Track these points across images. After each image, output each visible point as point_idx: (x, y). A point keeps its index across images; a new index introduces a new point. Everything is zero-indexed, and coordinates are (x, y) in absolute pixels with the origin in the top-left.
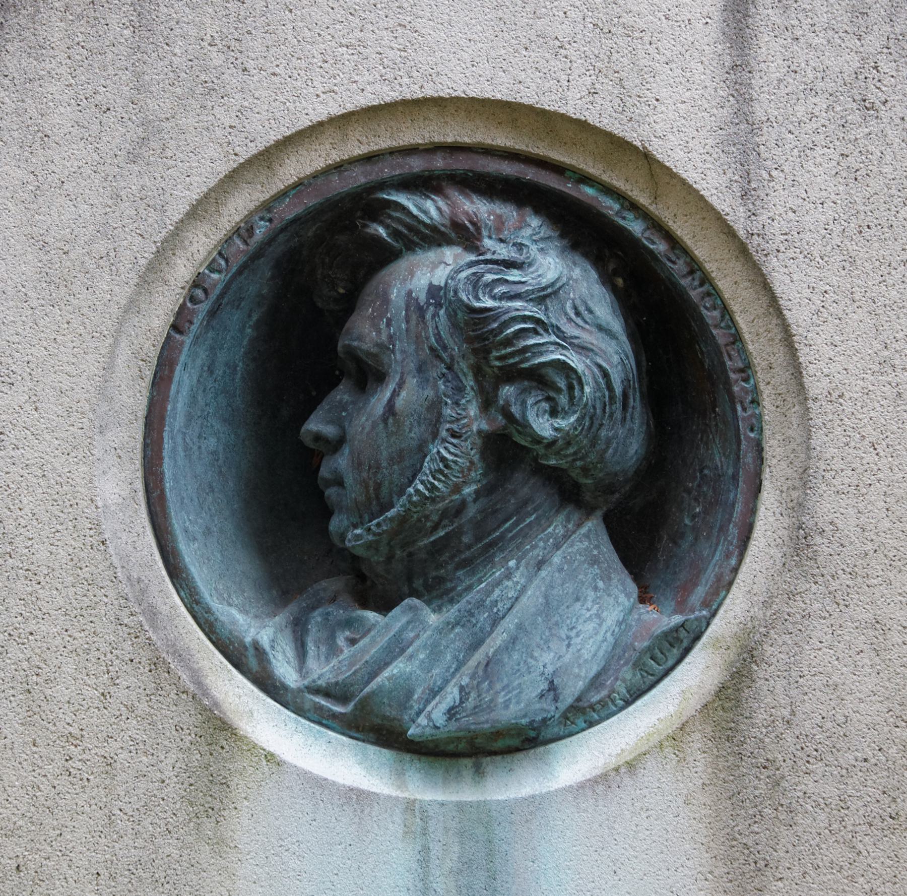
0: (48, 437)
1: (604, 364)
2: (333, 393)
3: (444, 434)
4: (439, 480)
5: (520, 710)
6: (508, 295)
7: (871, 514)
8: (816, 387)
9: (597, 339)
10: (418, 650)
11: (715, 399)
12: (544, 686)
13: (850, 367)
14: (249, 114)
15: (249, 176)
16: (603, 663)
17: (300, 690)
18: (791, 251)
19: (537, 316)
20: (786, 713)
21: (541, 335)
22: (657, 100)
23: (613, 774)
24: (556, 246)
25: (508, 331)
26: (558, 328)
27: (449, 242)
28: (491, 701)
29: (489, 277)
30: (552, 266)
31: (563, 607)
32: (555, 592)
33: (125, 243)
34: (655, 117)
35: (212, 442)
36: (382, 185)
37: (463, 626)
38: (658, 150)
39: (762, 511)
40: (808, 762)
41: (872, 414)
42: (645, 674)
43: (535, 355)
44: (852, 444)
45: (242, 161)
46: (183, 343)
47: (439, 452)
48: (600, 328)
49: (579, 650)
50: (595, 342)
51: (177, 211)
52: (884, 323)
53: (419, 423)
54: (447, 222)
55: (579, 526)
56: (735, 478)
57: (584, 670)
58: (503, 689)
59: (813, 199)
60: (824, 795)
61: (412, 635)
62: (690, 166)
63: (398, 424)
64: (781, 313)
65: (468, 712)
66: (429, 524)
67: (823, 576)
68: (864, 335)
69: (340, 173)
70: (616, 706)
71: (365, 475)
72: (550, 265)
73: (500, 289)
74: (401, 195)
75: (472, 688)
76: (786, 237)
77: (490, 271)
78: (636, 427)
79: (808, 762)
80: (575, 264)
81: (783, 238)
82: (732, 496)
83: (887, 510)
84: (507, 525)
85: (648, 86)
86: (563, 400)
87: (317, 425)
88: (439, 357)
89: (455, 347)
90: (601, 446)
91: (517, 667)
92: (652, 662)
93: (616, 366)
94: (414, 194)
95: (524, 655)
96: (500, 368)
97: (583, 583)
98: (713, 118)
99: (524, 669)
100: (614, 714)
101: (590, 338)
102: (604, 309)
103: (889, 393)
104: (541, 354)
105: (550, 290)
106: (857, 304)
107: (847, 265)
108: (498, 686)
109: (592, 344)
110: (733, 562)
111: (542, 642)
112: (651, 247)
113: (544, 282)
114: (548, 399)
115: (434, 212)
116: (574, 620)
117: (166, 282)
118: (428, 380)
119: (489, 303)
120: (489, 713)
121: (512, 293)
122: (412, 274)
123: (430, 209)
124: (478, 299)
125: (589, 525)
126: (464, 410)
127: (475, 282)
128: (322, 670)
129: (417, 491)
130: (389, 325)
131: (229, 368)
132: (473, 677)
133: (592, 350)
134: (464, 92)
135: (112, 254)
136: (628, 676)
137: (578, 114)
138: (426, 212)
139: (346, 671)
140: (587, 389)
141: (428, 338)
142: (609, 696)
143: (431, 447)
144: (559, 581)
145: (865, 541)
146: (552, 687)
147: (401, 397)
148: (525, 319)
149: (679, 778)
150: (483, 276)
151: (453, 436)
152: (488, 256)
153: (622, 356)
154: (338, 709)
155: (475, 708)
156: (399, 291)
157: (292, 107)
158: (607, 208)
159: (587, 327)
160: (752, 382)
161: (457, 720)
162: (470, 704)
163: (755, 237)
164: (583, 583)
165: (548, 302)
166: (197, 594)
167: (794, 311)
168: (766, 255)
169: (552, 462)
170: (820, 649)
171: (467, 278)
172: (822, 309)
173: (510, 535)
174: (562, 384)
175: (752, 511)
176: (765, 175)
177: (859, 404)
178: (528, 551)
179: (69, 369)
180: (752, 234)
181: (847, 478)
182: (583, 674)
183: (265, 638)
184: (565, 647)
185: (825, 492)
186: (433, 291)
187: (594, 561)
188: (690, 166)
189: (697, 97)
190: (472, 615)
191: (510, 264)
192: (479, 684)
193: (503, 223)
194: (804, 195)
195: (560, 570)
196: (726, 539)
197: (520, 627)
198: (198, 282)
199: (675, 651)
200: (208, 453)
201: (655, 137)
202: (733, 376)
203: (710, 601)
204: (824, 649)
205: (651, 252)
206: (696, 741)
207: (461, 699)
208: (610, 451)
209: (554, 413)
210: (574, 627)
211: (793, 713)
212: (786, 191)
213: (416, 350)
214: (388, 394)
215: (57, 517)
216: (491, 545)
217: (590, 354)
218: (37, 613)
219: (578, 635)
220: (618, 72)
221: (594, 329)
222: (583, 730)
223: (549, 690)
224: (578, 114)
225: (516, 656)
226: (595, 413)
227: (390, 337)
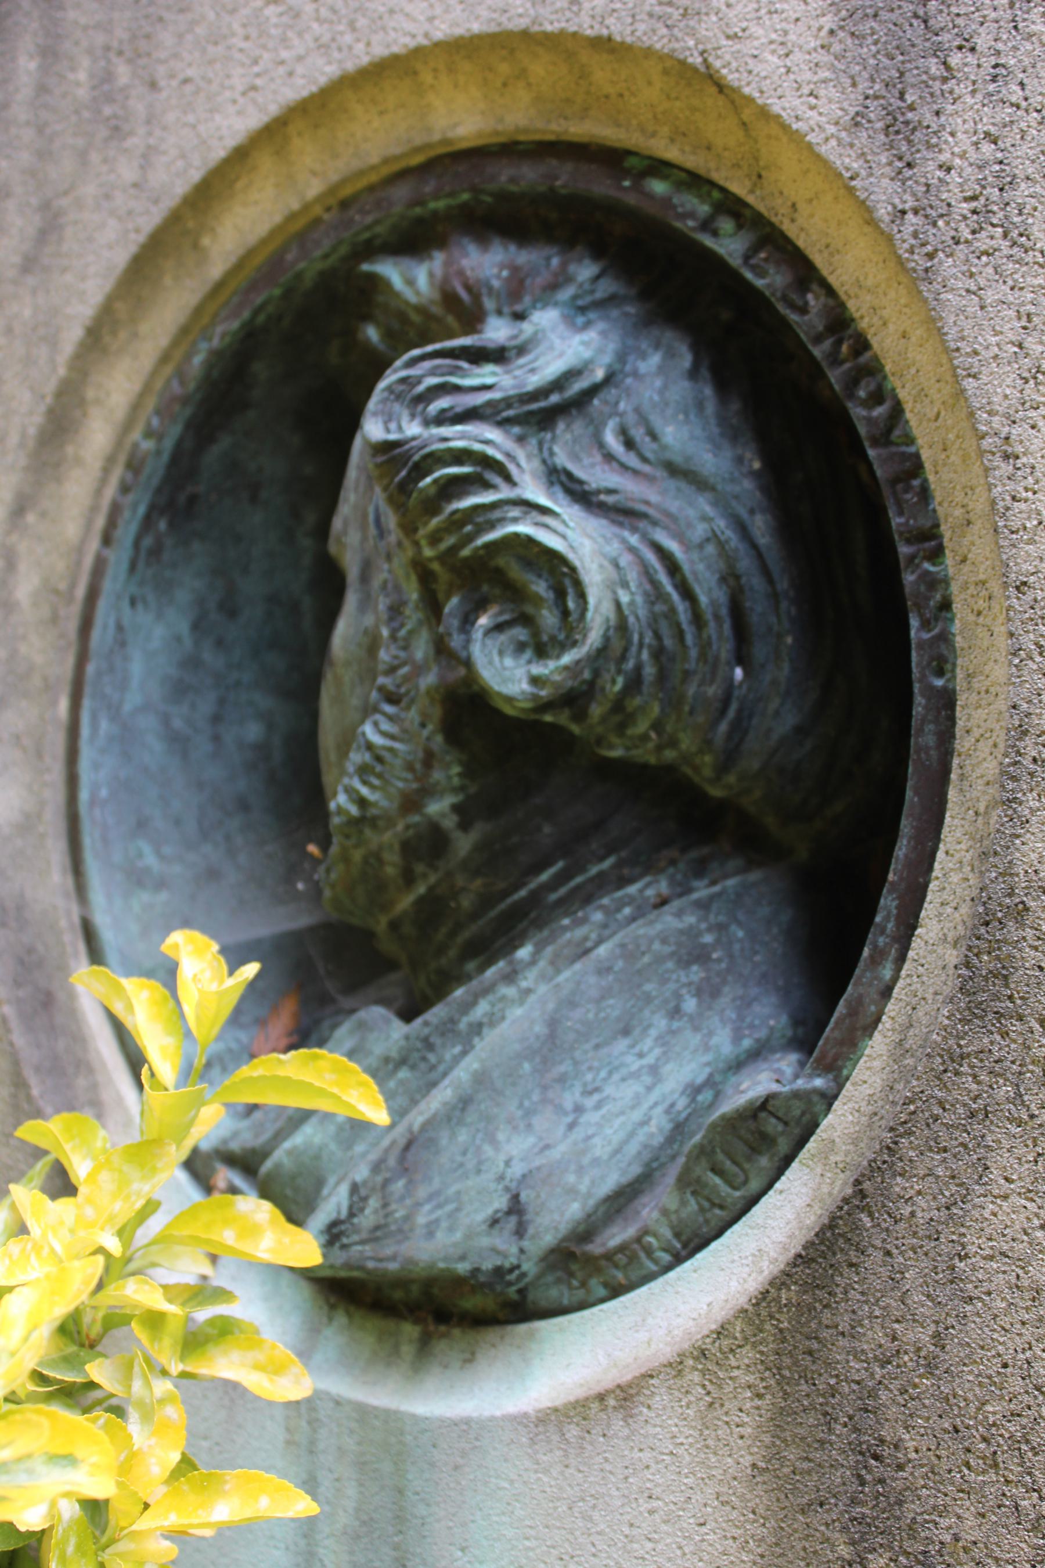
1: (673, 546)
5: (455, 1245)
6: (450, 414)
12: (501, 1203)
16: (636, 1170)
18: (984, 234)
20: (924, 1336)
23: (595, 1406)
24: (626, 314)
26: (569, 475)
28: (407, 1218)
31: (587, 1046)
32: (577, 1014)
35: (254, 731)
37: (413, 1067)
40: (968, 1465)
42: (706, 1205)
43: (480, 530)
48: (673, 470)
49: (589, 1138)
50: (654, 497)
51: (73, 335)
54: (436, 296)
57: (586, 1181)
58: (430, 1198)
60: (998, 1553)
65: (364, 1235)
67: (1020, 1018)
70: (656, 1261)
75: (373, 1189)
76: (974, 204)
77: (432, 373)
79: (968, 1465)
84: (545, 877)
91: (459, 1158)
92: (717, 1180)
93: (701, 546)
95: (480, 1135)
97: (648, 999)
99: (471, 1165)
100: (648, 1278)
104: (492, 525)
105: (554, 398)
108: (422, 1192)
109: (647, 503)
111: (520, 1113)
116: (603, 1074)
120: (399, 1242)
121: (458, 410)
123: (413, 280)
126: (405, 648)
132: (377, 1167)
133: (644, 516)
134: (426, 35)
136: (673, 1204)
137: (597, 27)
142: (639, 1240)
144: (594, 993)
146: (516, 1208)
148: (461, 456)
149: (711, 1442)
155: (377, 1228)
158: (684, 216)
159: (646, 468)
161: (344, 1247)
162: (367, 1219)
163: (910, 216)
167: (984, 379)
168: (931, 256)
169: (617, 753)
170: (1005, 1197)
173: (553, 897)
174: (540, 587)
176: (935, 67)
178: (565, 929)
180: (903, 212)
182: (583, 1188)
184: (561, 1129)
185: (1033, 811)
190: (430, 1046)
192: (386, 1183)
195: (604, 970)
197: (480, 1079)
199: (764, 1161)
201: (728, 37)
202: (904, 550)
203: (835, 1059)
204: (1014, 1199)
206: (743, 1369)
207: (351, 1207)
209: (541, 652)
210: (597, 1090)
212: (979, 96)
217: (642, 524)
219: (598, 1106)
221: (660, 473)
222: (603, 1300)
223: (509, 1212)
224: (597, 27)
225: (463, 1136)
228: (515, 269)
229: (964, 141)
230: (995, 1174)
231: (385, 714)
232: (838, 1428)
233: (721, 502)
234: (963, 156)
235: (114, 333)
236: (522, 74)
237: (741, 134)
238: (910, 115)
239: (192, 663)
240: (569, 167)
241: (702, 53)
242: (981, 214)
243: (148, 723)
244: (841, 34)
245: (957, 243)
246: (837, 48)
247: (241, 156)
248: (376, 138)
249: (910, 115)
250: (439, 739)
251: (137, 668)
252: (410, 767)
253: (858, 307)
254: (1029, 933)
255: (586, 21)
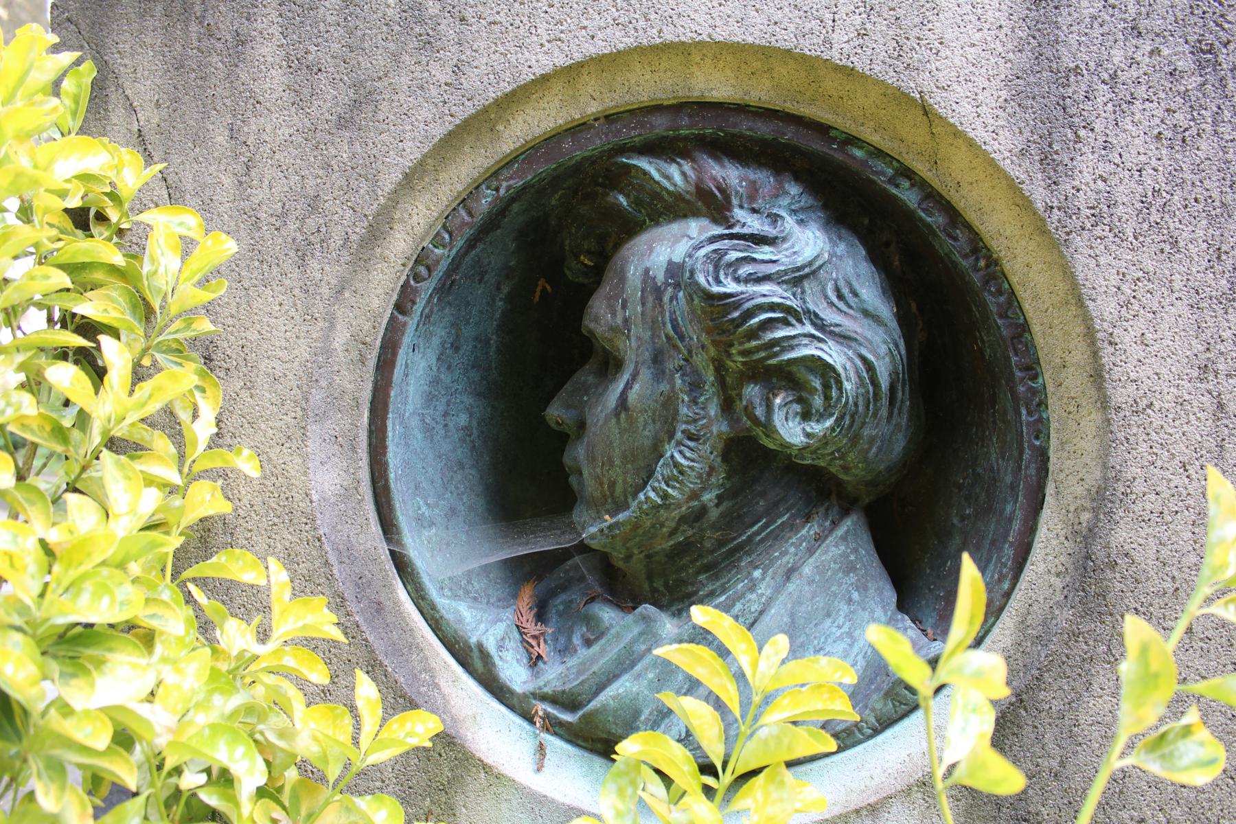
0: (263, 426)
1: (870, 357)
2: (578, 374)
3: (679, 435)
4: (673, 487)
7: (1176, 546)
8: (1120, 395)
9: (862, 326)
10: (646, 669)
11: (995, 393)
13: (1163, 371)
14: (466, 69)
15: (470, 139)
17: (525, 695)
19: (788, 303)
20: (1055, 764)
21: (792, 325)
22: (941, 43)
25: (752, 322)
26: (816, 315)
27: (696, 214)
29: (733, 255)
30: (811, 242)
32: (803, 608)
33: (336, 217)
34: (938, 64)
35: (463, 419)
36: (624, 150)
38: (938, 102)
39: (1042, 533)
41: (1185, 428)
43: (784, 350)
44: (1159, 463)
45: (458, 122)
46: (405, 324)
47: (672, 456)
48: (866, 313)
50: (859, 330)
51: (390, 179)
52: (1208, 318)
53: (654, 421)
54: (692, 189)
55: (835, 524)
56: (1013, 487)
59: (1128, 165)
61: (643, 647)
62: (978, 123)
63: (631, 421)
64: (1083, 303)
66: (665, 530)
67: (1111, 615)
68: (1183, 334)
69: (573, 134)
71: (598, 470)
72: (808, 241)
73: (744, 270)
74: (643, 159)
78: (904, 422)
80: (840, 238)
81: (1089, 212)
82: (1009, 508)
83: (1195, 542)
84: (756, 528)
85: (930, 26)
86: (818, 401)
87: (556, 412)
88: (675, 347)
89: (695, 334)
90: (863, 444)
94: (657, 157)
96: (744, 363)
97: (835, 595)
98: (1009, 65)
100: (860, 742)
101: (849, 325)
102: (871, 293)
103: (1208, 404)
104: (792, 348)
105: (807, 270)
106: (1176, 295)
107: (1167, 248)
110: (1006, 586)
112: (929, 219)
113: (800, 261)
114: (800, 400)
115: (677, 178)
117: (385, 259)
118: (664, 372)
119: (731, 287)
122: (651, 249)
123: (674, 175)
124: (718, 282)
125: (848, 524)
126: (703, 409)
127: (716, 261)
128: (554, 675)
129: (647, 498)
130: (624, 307)
131: (481, 341)
133: (856, 340)
134: (710, 36)
135: (323, 229)
136: (879, 706)
138: (668, 178)
139: (575, 679)
140: (847, 386)
141: (664, 324)
143: (667, 447)
144: (809, 596)
145: (1165, 577)
147: (634, 390)
148: (773, 307)
150: (726, 254)
151: (690, 439)
152: (736, 230)
153: (891, 346)
154: (567, 717)
156: (636, 269)
157: (513, 60)
159: (851, 312)
160: (1040, 380)
163: (1055, 210)
164: (835, 595)
165: (806, 284)
166: (422, 590)
167: (1099, 302)
168: (1068, 234)
171: (707, 256)
172: (1133, 300)
173: (759, 538)
174: (817, 383)
175: (1031, 529)
176: (1070, 135)
177: (1171, 416)
178: (777, 558)
179: (281, 354)
180: (1052, 208)
181: (1151, 503)
183: (491, 639)
186: (674, 270)
187: (850, 569)
188: (978, 123)
189: (989, 39)
191: (759, 240)
193: (757, 191)
194: (1118, 160)
195: (811, 582)
196: (999, 559)
198: (421, 258)
200: (458, 430)
202: (1018, 374)
204: (1106, 697)
205: (929, 226)
208: (874, 450)
209: (806, 416)
211: (1062, 764)
212: (1096, 155)
213: (653, 337)
214: (622, 386)
215: (274, 510)
216: (740, 547)
218: (259, 605)
220: (893, 9)
226: (857, 411)
227: (626, 320)
228: (753, 183)
229: (1088, 178)
230: (1096, 686)
231: (688, 447)
232: (1004, 810)
233: (888, 332)
234: (1087, 184)
235: (421, 178)
236: (770, 70)
237: (928, 138)
238: (1055, 157)
239: (435, 382)
240: (792, 128)
241: (920, 93)
242: (1097, 218)
243: (415, 422)
244: (1012, 103)
245: (1083, 229)
246: (1009, 110)
247: (544, 80)
248: (646, 86)
249: (1055, 157)
250: (719, 459)
251: (411, 389)
252: (700, 477)
253: (998, 246)
254: (1118, 575)
255: (837, 56)
